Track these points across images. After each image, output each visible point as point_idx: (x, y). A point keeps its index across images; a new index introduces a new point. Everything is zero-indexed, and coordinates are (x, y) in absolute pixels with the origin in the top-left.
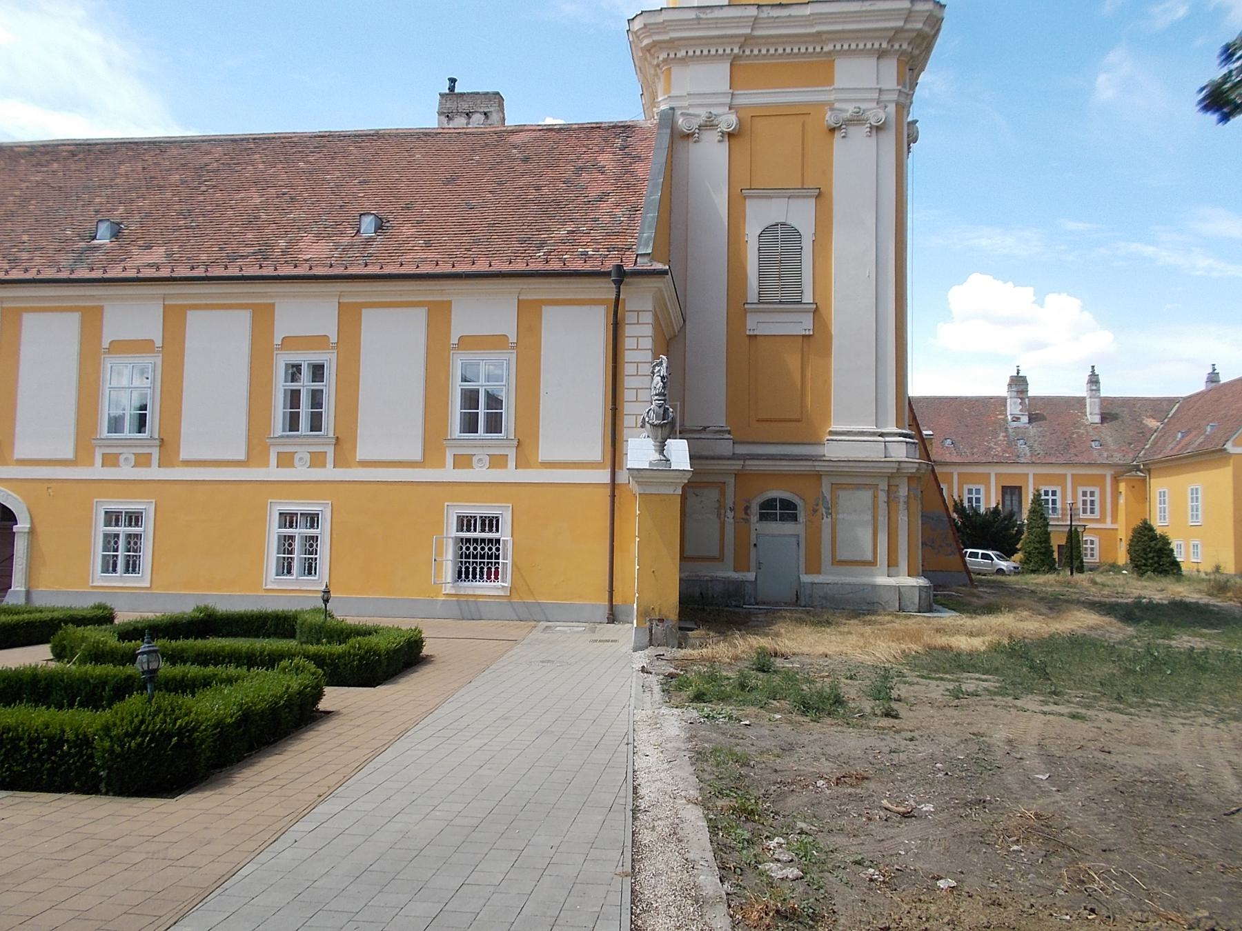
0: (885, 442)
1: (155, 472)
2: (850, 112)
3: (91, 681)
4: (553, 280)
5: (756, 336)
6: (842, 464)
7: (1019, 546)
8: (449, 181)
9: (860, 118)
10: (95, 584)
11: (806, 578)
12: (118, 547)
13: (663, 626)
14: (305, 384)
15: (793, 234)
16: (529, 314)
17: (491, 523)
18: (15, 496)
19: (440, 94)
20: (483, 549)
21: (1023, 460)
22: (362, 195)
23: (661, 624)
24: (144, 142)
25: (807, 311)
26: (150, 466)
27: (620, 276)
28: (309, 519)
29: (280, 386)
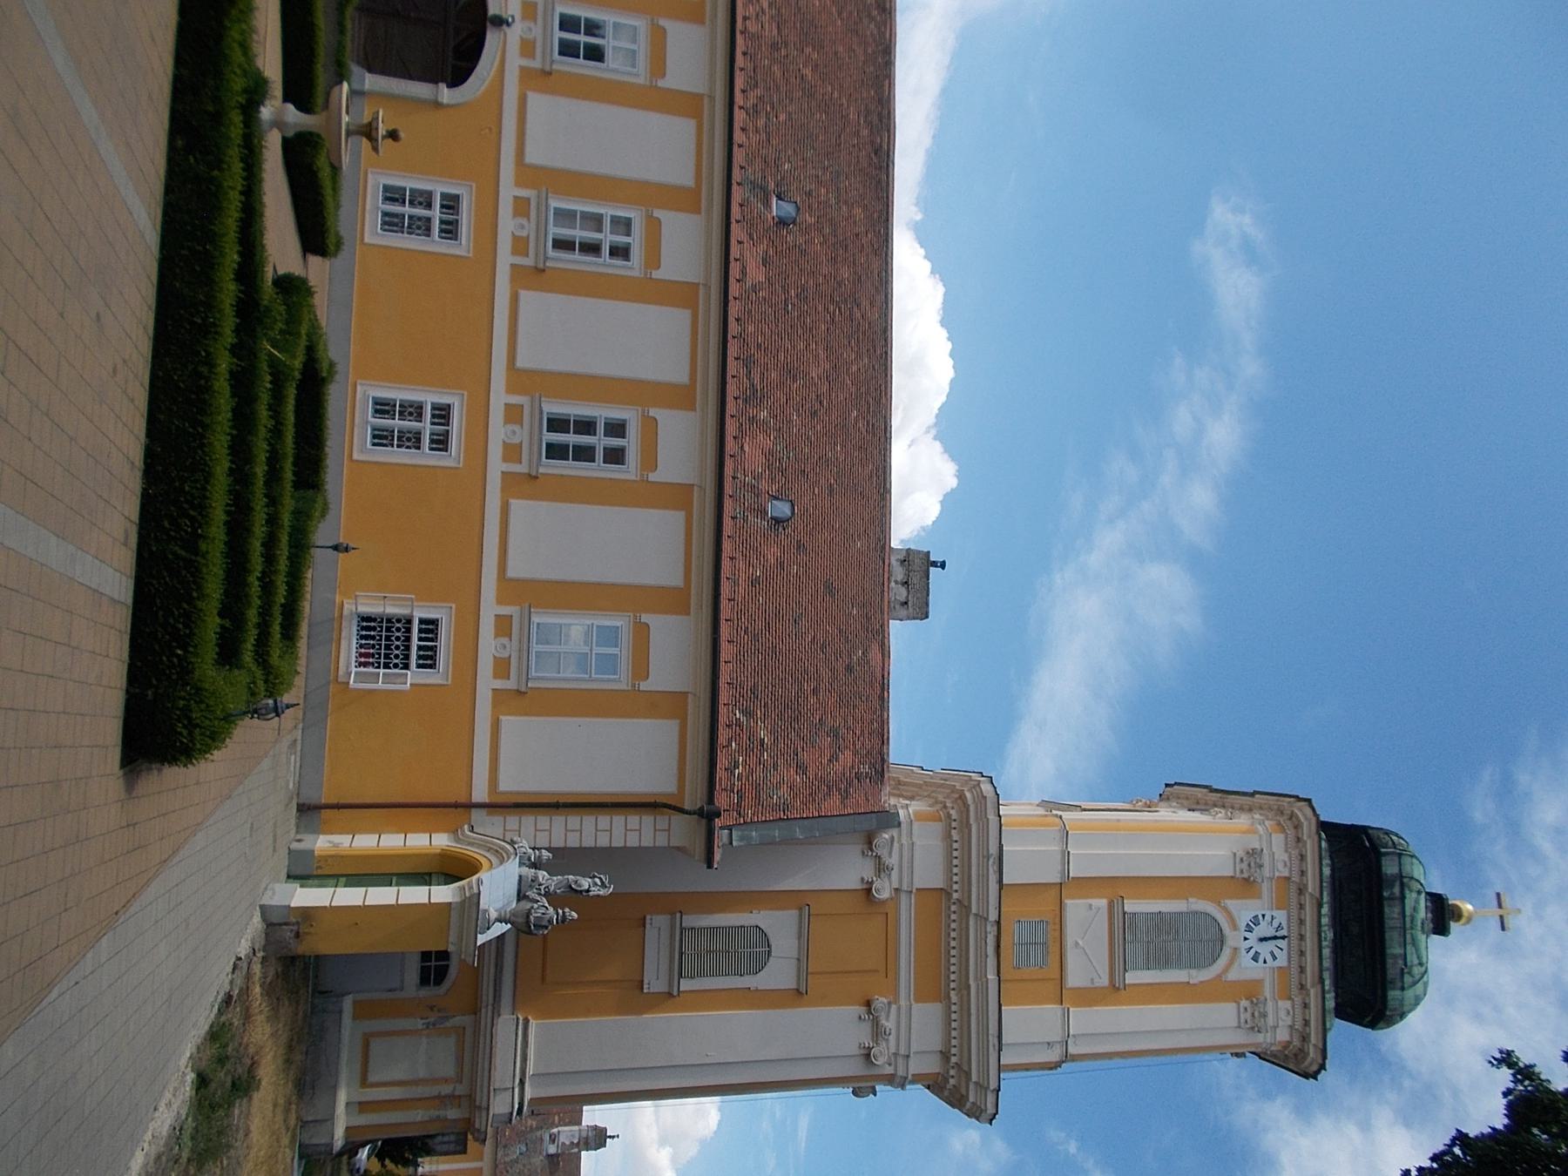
0: (513, 1088)
1: (505, 259)
2: (886, 1024)
3: (248, 466)
4: (707, 735)
5: (645, 927)
6: (488, 1041)
7: (387, 1162)
8: (829, 588)
9: (879, 1035)
10: (370, 176)
11: (348, 1004)
12: (390, 668)
13: (290, 938)
14: (602, 442)
15: (758, 963)
16: (669, 705)
17: (429, 659)
18: (483, 88)
19: (929, 552)
20: (397, 648)
21: (500, 1154)
22: (816, 492)
23: (292, 935)
24: (888, 228)
25: (670, 985)
26: (513, 253)
27: (708, 815)
28: (441, 438)
29: (601, 412)
